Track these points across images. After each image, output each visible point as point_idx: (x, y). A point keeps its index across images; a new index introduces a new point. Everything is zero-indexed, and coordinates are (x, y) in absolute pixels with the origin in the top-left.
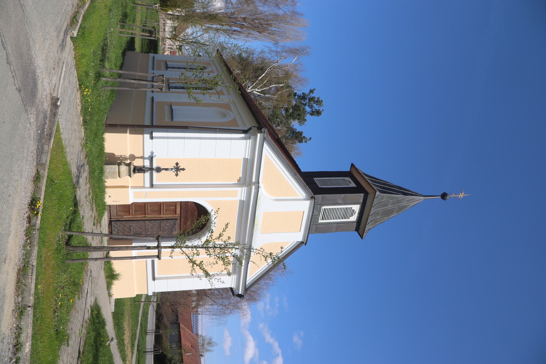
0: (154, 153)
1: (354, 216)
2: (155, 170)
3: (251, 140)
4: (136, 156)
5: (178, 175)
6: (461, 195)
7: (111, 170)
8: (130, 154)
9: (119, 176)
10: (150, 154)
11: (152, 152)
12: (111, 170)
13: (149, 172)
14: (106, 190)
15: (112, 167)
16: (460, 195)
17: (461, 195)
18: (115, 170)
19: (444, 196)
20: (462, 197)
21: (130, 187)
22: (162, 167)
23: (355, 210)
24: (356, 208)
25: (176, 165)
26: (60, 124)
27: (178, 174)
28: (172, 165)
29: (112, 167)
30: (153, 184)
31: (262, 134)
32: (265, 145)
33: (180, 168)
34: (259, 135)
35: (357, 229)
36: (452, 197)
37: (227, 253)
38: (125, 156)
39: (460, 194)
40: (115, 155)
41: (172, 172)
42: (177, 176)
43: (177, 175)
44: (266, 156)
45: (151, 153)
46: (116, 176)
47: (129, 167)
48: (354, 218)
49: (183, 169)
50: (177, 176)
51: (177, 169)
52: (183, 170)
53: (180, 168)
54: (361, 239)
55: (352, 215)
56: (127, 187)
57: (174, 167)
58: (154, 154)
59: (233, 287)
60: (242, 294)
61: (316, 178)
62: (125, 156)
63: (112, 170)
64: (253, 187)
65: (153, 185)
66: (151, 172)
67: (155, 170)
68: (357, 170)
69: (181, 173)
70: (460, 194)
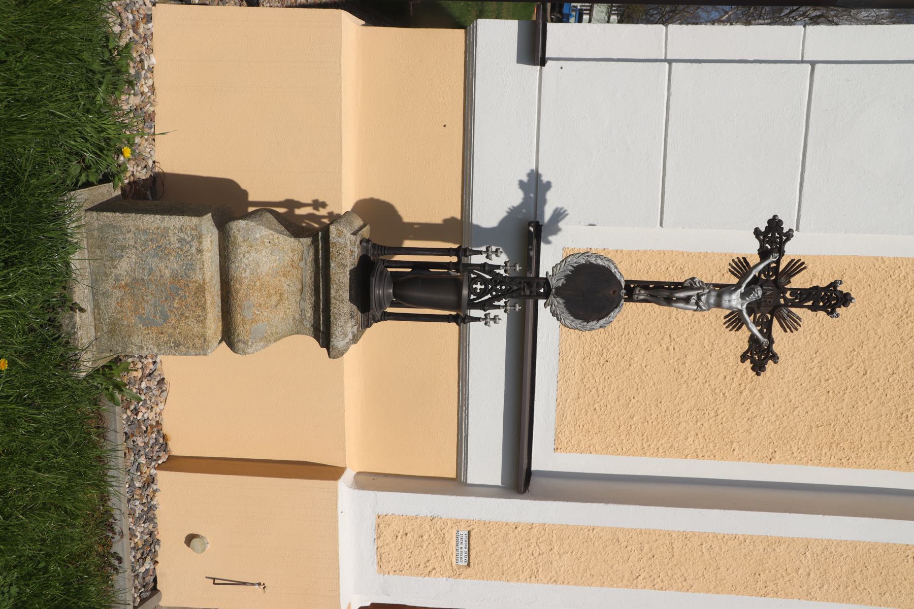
0: (548, 185)
2: (560, 292)
4: (407, 218)
5: (775, 358)
7: (153, 262)
8: (367, 196)
9: (229, 336)
10: (516, 198)
11: (535, 176)
12: (153, 262)
13: (500, 313)
15: (164, 233)
18: (190, 267)
21: (349, 475)
22: (626, 272)
25: (764, 254)
27: (776, 348)
29: (164, 233)
30: (534, 467)
33: (798, 282)
38: (323, 212)
40: (245, 193)
41: (717, 316)
42: (759, 368)
45: (522, 184)
46: (196, 329)
47: (315, 242)
50: (759, 368)
53: (798, 282)
54: (352, 604)
56: (333, 473)
57: (741, 267)
58: (550, 195)
62: (323, 212)
63: (167, 268)
65: (529, 473)
66: (523, 312)
67: (560, 292)
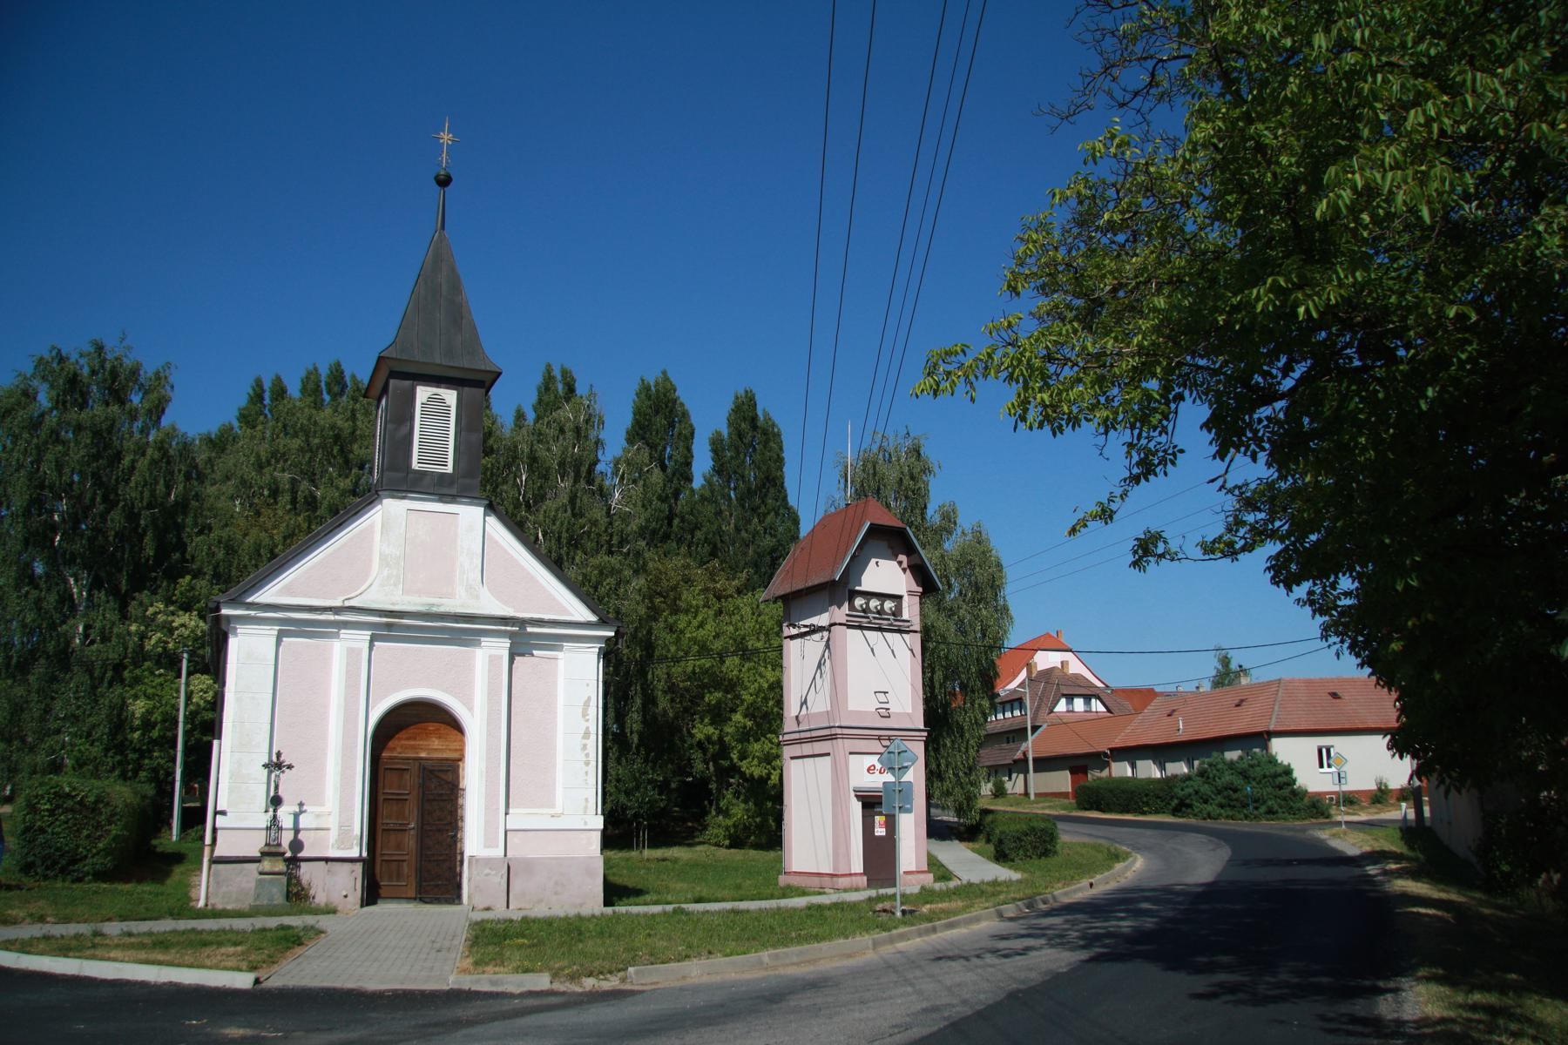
1: (444, 396)
6: (446, 138)
14: (1407, 759)
16: (443, 143)
17: (446, 138)
23: (429, 394)
24: (423, 393)
26: (1106, 874)
31: (221, 605)
32: (250, 600)
34: (225, 611)
37: (1225, 482)
44: (281, 593)
48: (450, 396)
60: (615, 629)
64: (530, 629)
69: (286, 759)
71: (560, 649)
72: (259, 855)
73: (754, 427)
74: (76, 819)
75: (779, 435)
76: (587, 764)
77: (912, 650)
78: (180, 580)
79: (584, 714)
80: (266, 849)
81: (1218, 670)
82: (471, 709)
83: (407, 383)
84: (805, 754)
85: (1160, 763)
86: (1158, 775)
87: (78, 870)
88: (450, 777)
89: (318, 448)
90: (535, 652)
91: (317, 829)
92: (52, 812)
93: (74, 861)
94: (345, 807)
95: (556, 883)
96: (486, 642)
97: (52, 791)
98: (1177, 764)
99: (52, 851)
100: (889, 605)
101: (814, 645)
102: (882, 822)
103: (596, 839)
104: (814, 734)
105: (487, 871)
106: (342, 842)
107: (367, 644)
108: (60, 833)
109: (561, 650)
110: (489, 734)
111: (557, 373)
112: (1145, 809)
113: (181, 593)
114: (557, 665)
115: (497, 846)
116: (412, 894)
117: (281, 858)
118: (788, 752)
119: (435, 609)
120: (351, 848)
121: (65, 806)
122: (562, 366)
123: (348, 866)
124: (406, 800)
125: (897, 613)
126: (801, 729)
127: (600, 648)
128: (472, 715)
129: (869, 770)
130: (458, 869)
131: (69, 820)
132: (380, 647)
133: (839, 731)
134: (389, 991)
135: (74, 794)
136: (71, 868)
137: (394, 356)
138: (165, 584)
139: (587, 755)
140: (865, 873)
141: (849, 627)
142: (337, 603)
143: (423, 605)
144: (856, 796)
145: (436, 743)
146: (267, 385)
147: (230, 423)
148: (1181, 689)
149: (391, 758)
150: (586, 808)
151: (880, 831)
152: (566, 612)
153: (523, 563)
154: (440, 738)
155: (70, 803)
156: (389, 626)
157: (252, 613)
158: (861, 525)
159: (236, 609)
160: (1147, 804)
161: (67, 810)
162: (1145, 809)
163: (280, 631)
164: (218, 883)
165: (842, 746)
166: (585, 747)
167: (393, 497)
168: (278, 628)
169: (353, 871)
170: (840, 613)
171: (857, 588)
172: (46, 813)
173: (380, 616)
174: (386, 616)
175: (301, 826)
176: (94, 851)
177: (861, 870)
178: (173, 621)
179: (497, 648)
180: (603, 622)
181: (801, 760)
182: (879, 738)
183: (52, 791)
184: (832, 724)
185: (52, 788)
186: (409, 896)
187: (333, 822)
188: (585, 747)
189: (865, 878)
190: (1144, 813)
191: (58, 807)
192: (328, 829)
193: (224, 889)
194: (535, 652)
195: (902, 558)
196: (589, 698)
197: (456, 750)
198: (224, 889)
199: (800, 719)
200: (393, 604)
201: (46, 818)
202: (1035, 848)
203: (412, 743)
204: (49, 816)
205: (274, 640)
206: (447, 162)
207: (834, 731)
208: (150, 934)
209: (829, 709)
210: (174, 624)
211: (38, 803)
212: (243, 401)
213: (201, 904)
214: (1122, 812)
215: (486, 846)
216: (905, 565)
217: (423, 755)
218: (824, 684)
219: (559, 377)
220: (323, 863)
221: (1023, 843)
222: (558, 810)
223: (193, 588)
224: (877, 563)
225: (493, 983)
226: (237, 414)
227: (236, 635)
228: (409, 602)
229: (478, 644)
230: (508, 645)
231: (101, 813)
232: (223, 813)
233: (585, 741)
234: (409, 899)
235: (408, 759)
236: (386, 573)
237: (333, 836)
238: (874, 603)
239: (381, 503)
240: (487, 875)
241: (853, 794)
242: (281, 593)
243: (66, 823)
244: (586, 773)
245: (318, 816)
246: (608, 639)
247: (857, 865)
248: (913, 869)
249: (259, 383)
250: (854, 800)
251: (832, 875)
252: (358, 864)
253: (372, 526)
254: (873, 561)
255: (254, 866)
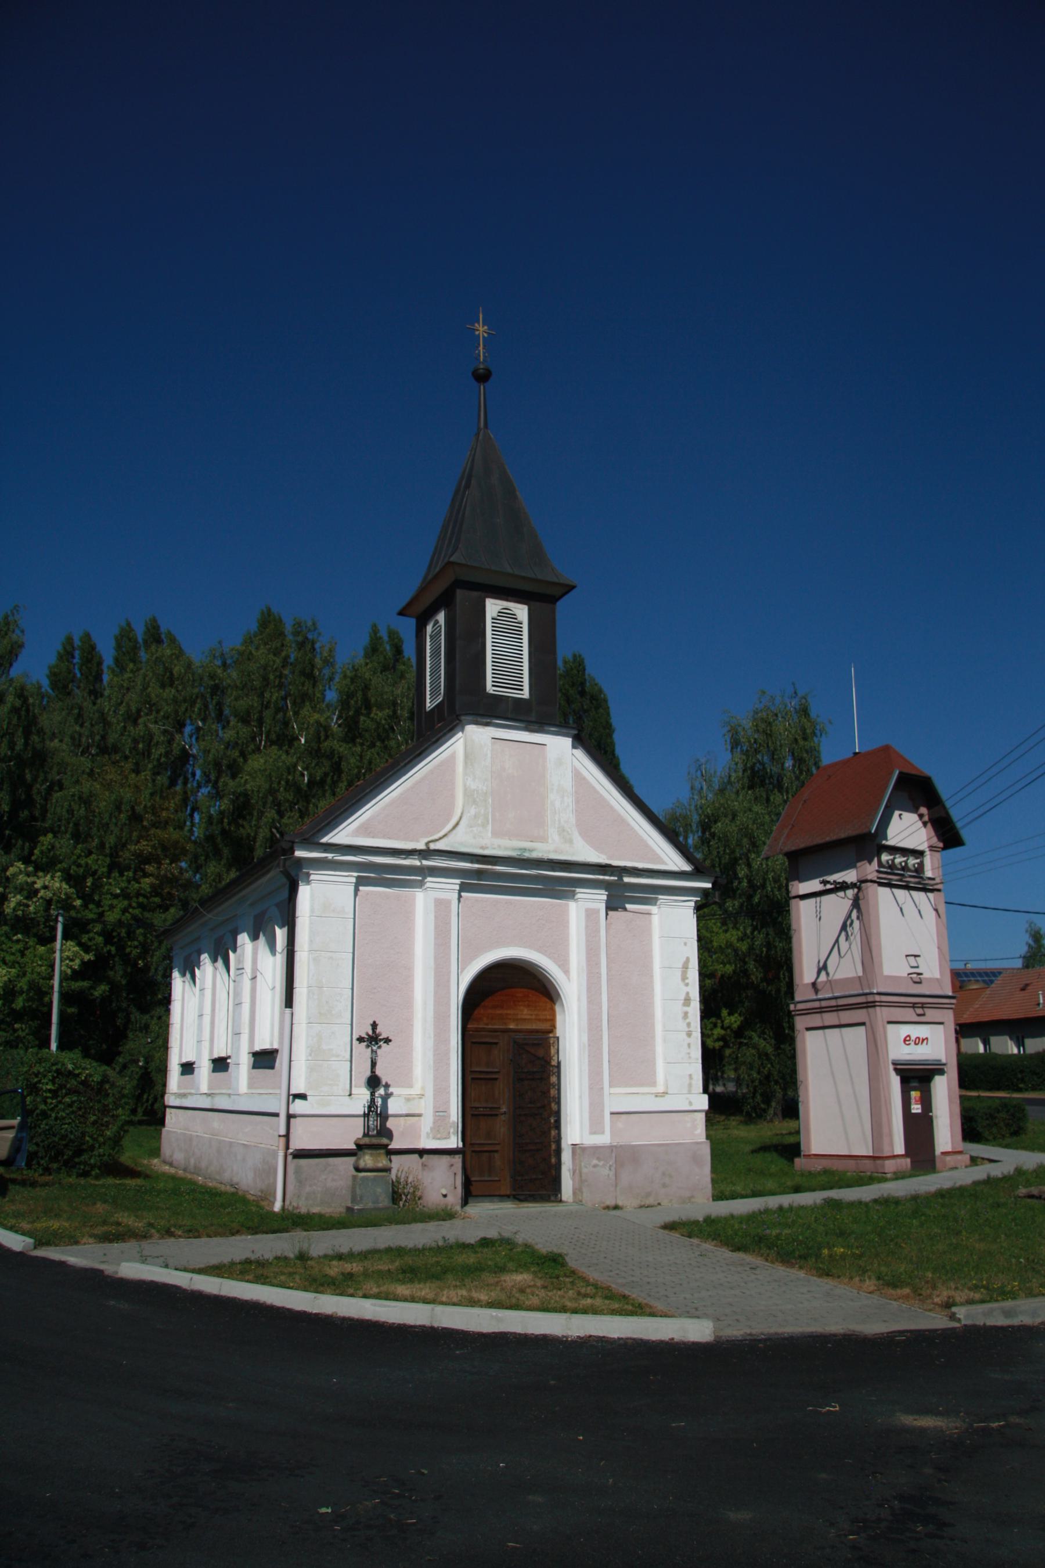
1: (516, 611)
3: (311, 872)
6: (481, 330)
19: (482, 377)
20: (486, 327)
22: (368, 1073)
23: (498, 608)
24: (493, 607)
28: (363, 1052)
32: (324, 840)
33: (370, 1033)
34: (299, 853)
35: (553, 600)
36: (484, 353)
39: (477, 333)
42: (390, 1041)
43: (387, 1041)
44: (358, 832)
48: (522, 612)
49: (374, 1025)
50: (390, 1041)
51: (373, 1039)
52: (376, 1025)
54: (575, 590)
55: (513, 616)
57: (368, 1046)
59: (692, 904)
60: (713, 879)
61: (428, 705)
64: (626, 880)
68: (409, 604)
69: (383, 1031)
70: (477, 333)
71: (652, 902)
72: (354, 1147)
73: (582, 693)
74: (81, 1102)
75: (606, 701)
76: (689, 1034)
77: (936, 910)
78: (42, 838)
79: (684, 978)
80: (367, 1141)
81: (1029, 945)
82: (567, 972)
83: (475, 594)
84: (843, 1022)
85: (1018, 1038)
86: (1015, 1051)
87: (85, 1163)
88: (541, 1053)
89: (197, 697)
90: (628, 906)
91: (407, 1115)
92: (55, 1093)
93: (79, 1152)
94: (440, 1090)
95: (664, 1174)
96: (582, 893)
97: (54, 1068)
98: (973, 1040)
99: (56, 1139)
100: (912, 862)
101: (838, 905)
102: (917, 1099)
103: (700, 1121)
104: (841, 1002)
105: (595, 1162)
106: (437, 1131)
107: (456, 895)
108: (64, 1118)
109: (655, 904)
110: (590, 1001)
111: (383, 634)
112: (1021, 1086)
113: (42, 852)
114: (650, 922)
115: (603, 1133)
116: (506, 1189)
117: (383, 1151)
118: (800, 1023)
119: (527, 855)
120: (448, 1137)
121: (68, 1086)
122: (389, 626)
123: (445, 1160)
124: (496, 1079)
125: (920, 869)
126: (820, 996)
127: (696, 902)
128: (569, 979)
129: (905, 1040)
130: (553, 1160)
131: (73, 1102)
132: (467, 898)
133: (877, 998)
134: (901, 1333)
135: (77, 1072)
136: (77, 1160)
137: (463, 562)
138: (20, 842)
139: (689, 1025)
140: (907, 1154)
141: (881, 884)
142: (421, 846)
143: (514, 849)
144: (896, 1070)
145: (526, 1011)
146: (77, 642)
147: (38, 683)
148: (969, 966)
149: (477, 1030)
150: (690, 1085)
151: (916, 1108)
152: (659, 860)
153: (613, 802)
154: (529, 1006)
155: (73, 1083)
156: (479, 874)
157: (330, 856)
158: (891, 773)
159: (311, 851)
160: (1022, 1080)
161: (70, 1092)
162: (1021, 1086)
163: (358, 878)
164: (300, 1182)
165: (882, 1014)
166: (686, 1015)
167: (477, 723)
168: (356, 874)
169: (452, 1165)
170: (870, 869)
171: (884, 842)
172: (49, 1095)
173: (472, 862)
174: (478, 862)
175: (391, 1111)
176: (101, 1139)
177: (903, 1152)
178: (35, 883)
179: (594, 899)
180: (698, 872)
181: (820, 1032)
182: (914, 1006)
183: (54, 1068)
184: (867, 991)
185: (53, 1065)
186: (502, 1193)
187: (426, 1107)
188: (686, 1015)
189: (908, 1160)
190: (1020, 1090)
191: (62, 1087)
192: (420, 1115)
193: (308, 1189)
194: (628, 906)
195: (923, 810)
196: (688, 959)
197: (546, 1020)
198: (308, 1189)
199: (819, 987)
200: (482, 848)
201: (49, 1101)
202: (1007, 1125)
203: (499, 1012)
204: (52, 1098)
205: (352, 888)
206: (484, 356)
207: (870, 998)
208: (399, 1252)
209: (860, 974)
210: (36, 886)
211: (39, 1082)
212: (52, 660)
213: (277, 1207)
214: (990, 1090)
215: (592, 1133)
216: (926, 818)
217: (512, 1026)
218: (853, 948)
219: (386, 638)
220: (416, 1156)
221: (997, 1121)
222: (660, 1089)
223: (53, 847)
224: (900, 815)
225: (1007, 1314)
226: (47, 672)
227: (308, 882)
228: (499, 846)
229: (571, 896)
230: (605, 897)
231: (108, 1095)
232: (303, 1097)
233: (686, 1009)
234: (504, 1197)
235: (495, 1031)
236: (473, 811)
237: (427, 1123)
238: (899, 860)
239: (462, 730)
240: (595, 1166)
241: (891, 1067)
242: (358, 832)
243: (70, 1105)
244: (689, 1045)
245: (408, 1099)
246: (705, 892)
247: (900, 1148)
248: (949, 1149)
249: (69, 640)
250: (893, 1074)
251: (873, 1158)
252: (457, 1156)
253: (453, 757)
254: (897, 813)
255: (351, 1160)
